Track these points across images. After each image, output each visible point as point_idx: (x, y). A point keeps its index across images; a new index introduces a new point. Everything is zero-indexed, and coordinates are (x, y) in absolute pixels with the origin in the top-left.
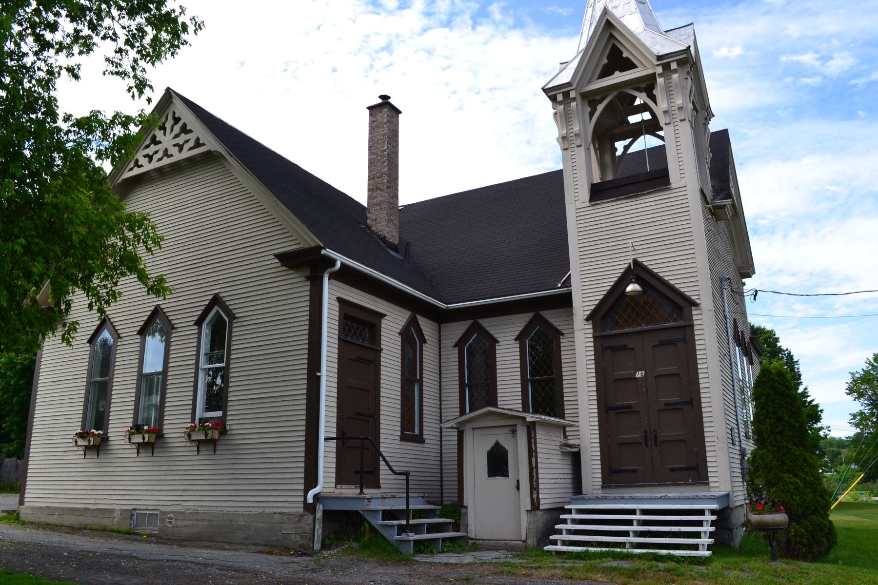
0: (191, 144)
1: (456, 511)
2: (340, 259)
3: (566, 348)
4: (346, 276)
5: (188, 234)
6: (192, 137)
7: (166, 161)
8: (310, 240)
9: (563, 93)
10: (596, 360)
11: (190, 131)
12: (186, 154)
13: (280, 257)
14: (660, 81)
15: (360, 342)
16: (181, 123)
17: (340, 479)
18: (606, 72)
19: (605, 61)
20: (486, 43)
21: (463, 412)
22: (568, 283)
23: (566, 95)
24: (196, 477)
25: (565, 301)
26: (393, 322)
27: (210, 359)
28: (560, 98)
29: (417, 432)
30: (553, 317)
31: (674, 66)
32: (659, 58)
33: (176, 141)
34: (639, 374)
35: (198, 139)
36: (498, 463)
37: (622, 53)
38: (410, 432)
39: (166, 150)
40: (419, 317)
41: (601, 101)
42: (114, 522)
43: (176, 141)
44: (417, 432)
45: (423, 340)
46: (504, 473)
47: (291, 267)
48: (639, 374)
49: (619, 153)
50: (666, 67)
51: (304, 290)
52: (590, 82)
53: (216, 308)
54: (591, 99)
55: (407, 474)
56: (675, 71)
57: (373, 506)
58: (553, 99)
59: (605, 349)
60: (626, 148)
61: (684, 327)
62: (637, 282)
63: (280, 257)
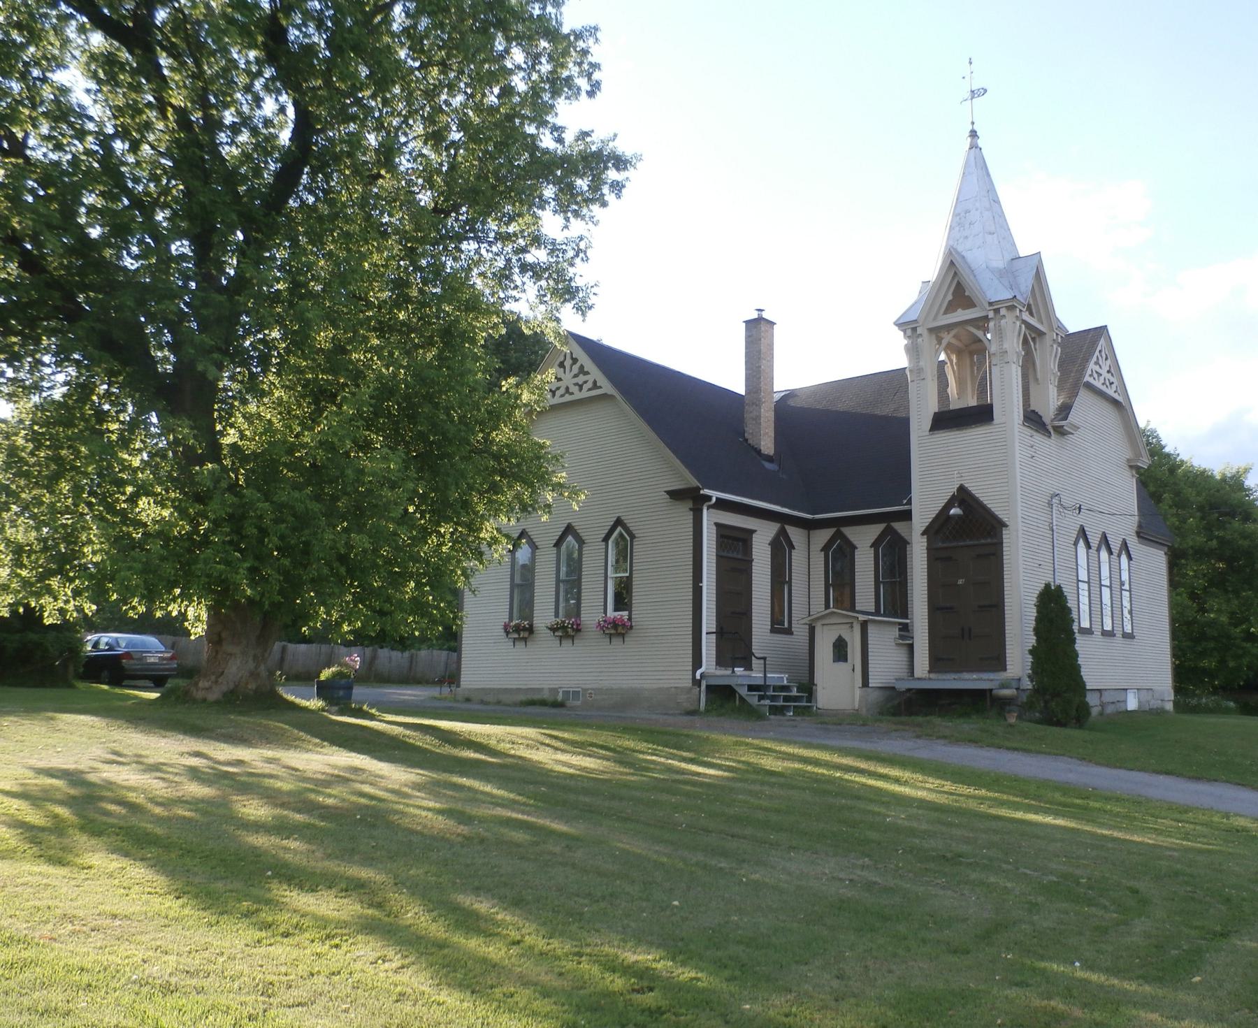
0: (590, 385)
1: (808, 688)
2: (715, 494)
4: (722, 505)
5: (593, 471)
6: (590, 378)
7: (568, 398)
8: (695, 483)
10: (929, 568)
11: (587, 373)
12: (585, 394)
13: (668, 492)
15: (735, 555)
16: (578, 365)
17: (720, 662)
18: (951, 308)
19: (950, 297)
21: (827, 606)
22: (909, 502)
25: (907, 516)
26: (763, 536)
27: (616, 570)
29: (786, 625)
30: (899, 526)
32: (991, 304)
33: (576, 380)
34: (960, 582)
35: (595, 382)
36: (840, 650)
38: (779, 625)
39: (567, 388)
40: (787, 527)
42: (546, 696)
43: (576, 380)
44: (786, 625)
45: (792, 547)
46: (846, 660)
47: (676, 499)
48: (960, 582)
50: (997, 311)
51: (689, 517)
53: (619, 529)
55: (764, 659)
57: (740, 681)
59: (934, 557)
61: (995, 544)
62: (959, 506)
63: (668, 492)
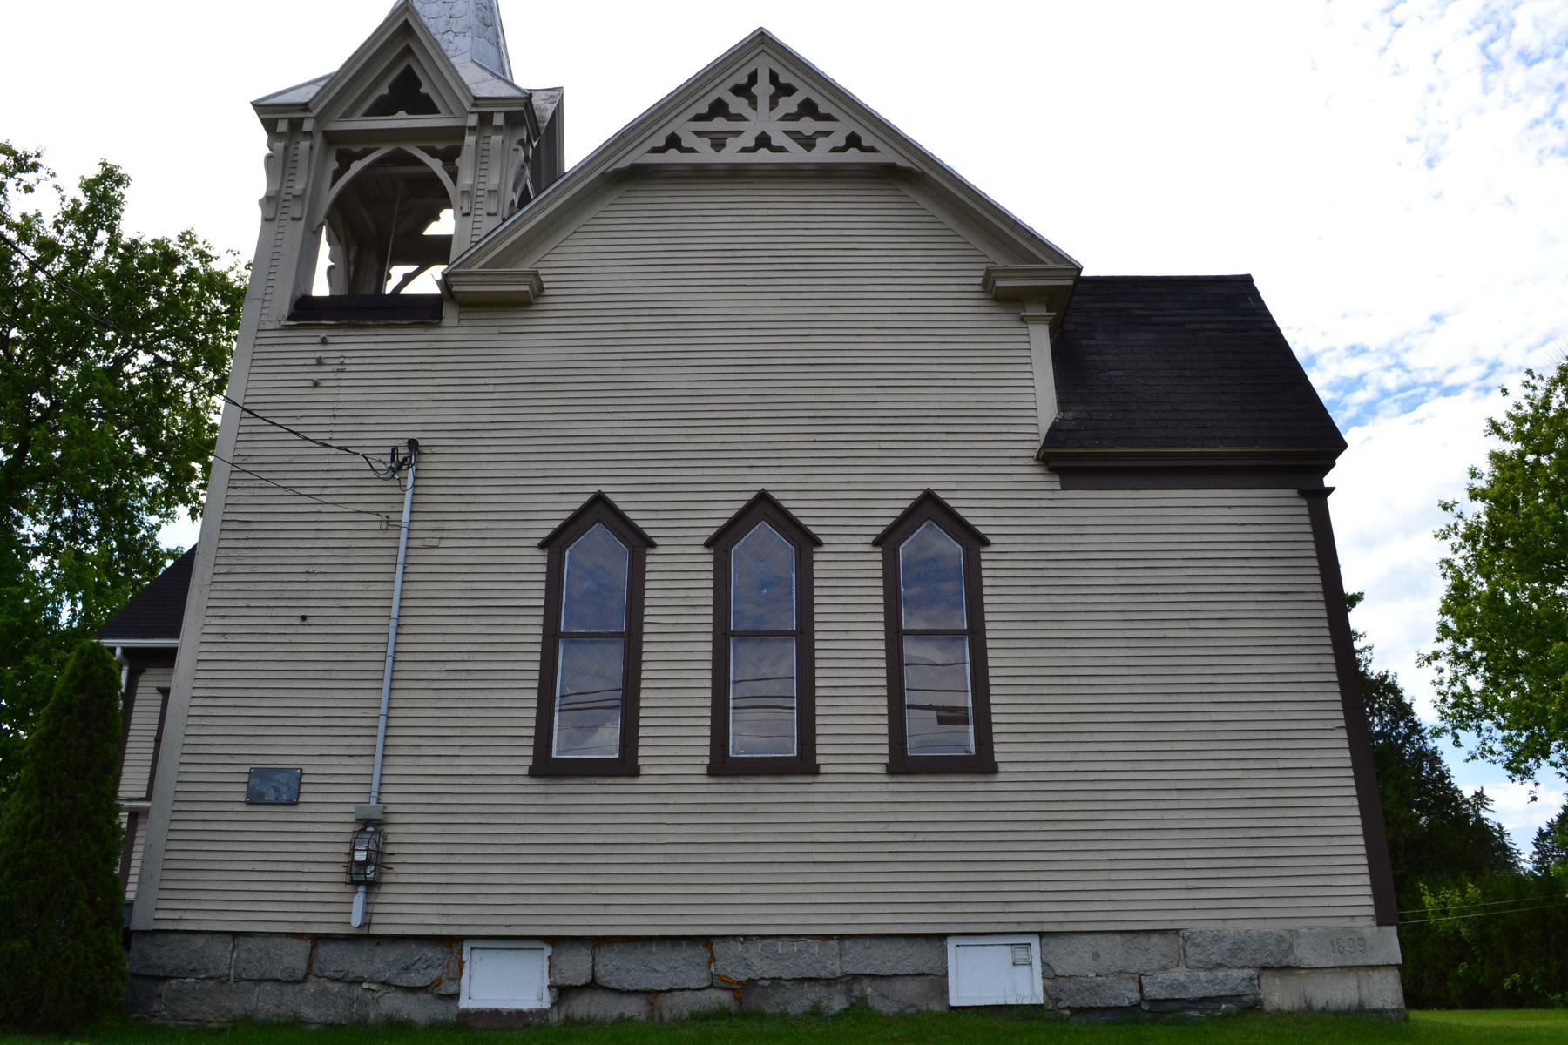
3: (702, 602)
9: (291, 120)
14: (470, 140)
18: (384, 108)
20: (1442, 16)
23: (296, 125)
24: (416, 799)
28: (283, 127)
31: (499, 120)
37: (420, 85)
41: (360, 156)
49: (389, 288)
50: (486, 119)
52: (348, 115)
54: (342, 147)
56: (498, 129)
58: (270, 126)
60: (408, 278)
